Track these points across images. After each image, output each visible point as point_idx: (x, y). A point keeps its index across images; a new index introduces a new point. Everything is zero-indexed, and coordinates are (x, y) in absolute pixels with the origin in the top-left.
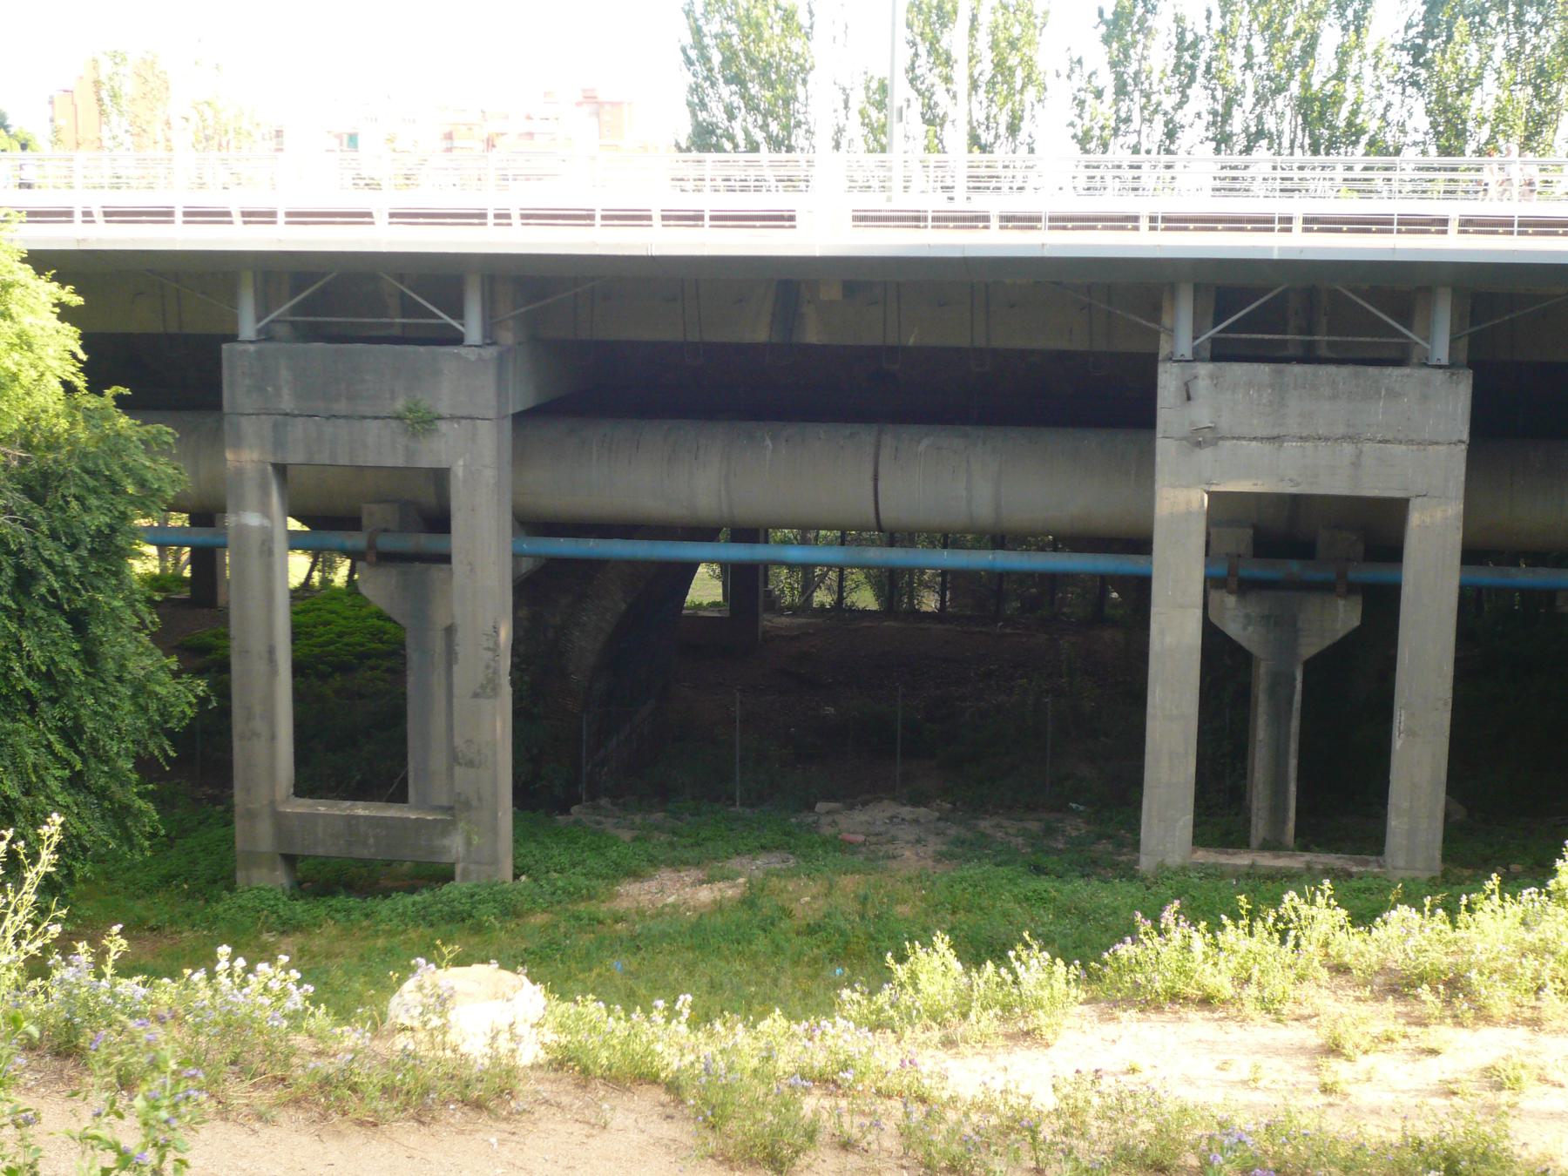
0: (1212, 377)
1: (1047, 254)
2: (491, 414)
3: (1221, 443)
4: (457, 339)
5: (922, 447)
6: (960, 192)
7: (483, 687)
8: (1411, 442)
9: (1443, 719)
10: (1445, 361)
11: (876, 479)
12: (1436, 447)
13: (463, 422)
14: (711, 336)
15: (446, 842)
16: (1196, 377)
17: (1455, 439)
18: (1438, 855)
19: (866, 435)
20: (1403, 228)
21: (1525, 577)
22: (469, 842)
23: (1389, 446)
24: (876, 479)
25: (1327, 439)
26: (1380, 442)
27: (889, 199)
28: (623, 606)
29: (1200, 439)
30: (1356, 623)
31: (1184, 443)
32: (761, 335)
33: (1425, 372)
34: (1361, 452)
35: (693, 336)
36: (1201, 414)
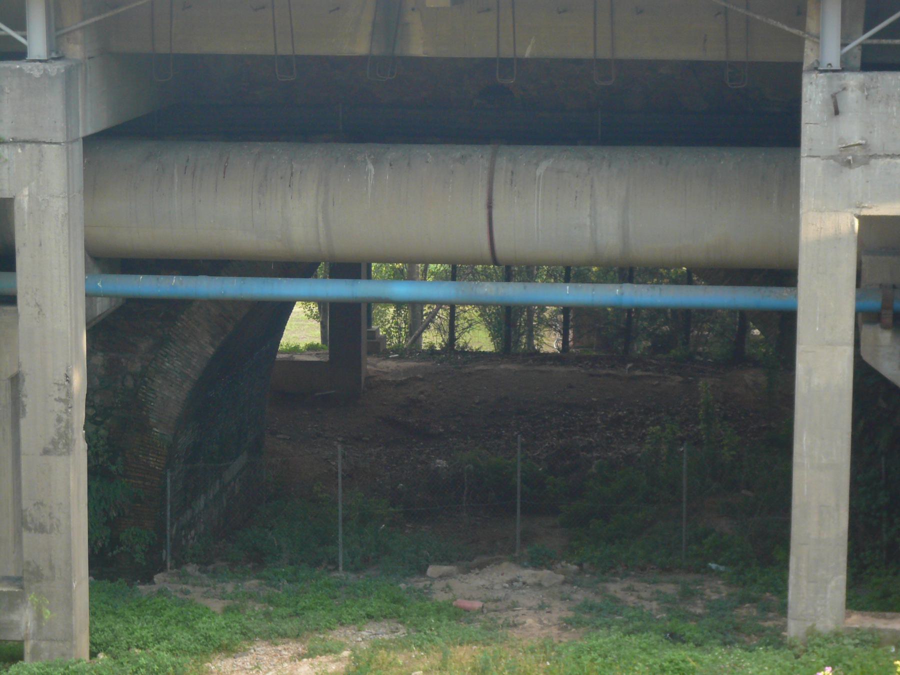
0: (863, 87)
2: (60, 137)
3: (873, 161)
4: (20, 54)
5: (540, 171)
7: (53, 442)
11: (490, 206)
13: (28, 146)
14: (307, 48)
15: (15, 617)
16: (844, 89)
19: (479, 156)
22: (39, 617)
24: (490, 206)
28: (211, 350)
31: (832, 161)
32: (362, 48)
35: (285, 49)
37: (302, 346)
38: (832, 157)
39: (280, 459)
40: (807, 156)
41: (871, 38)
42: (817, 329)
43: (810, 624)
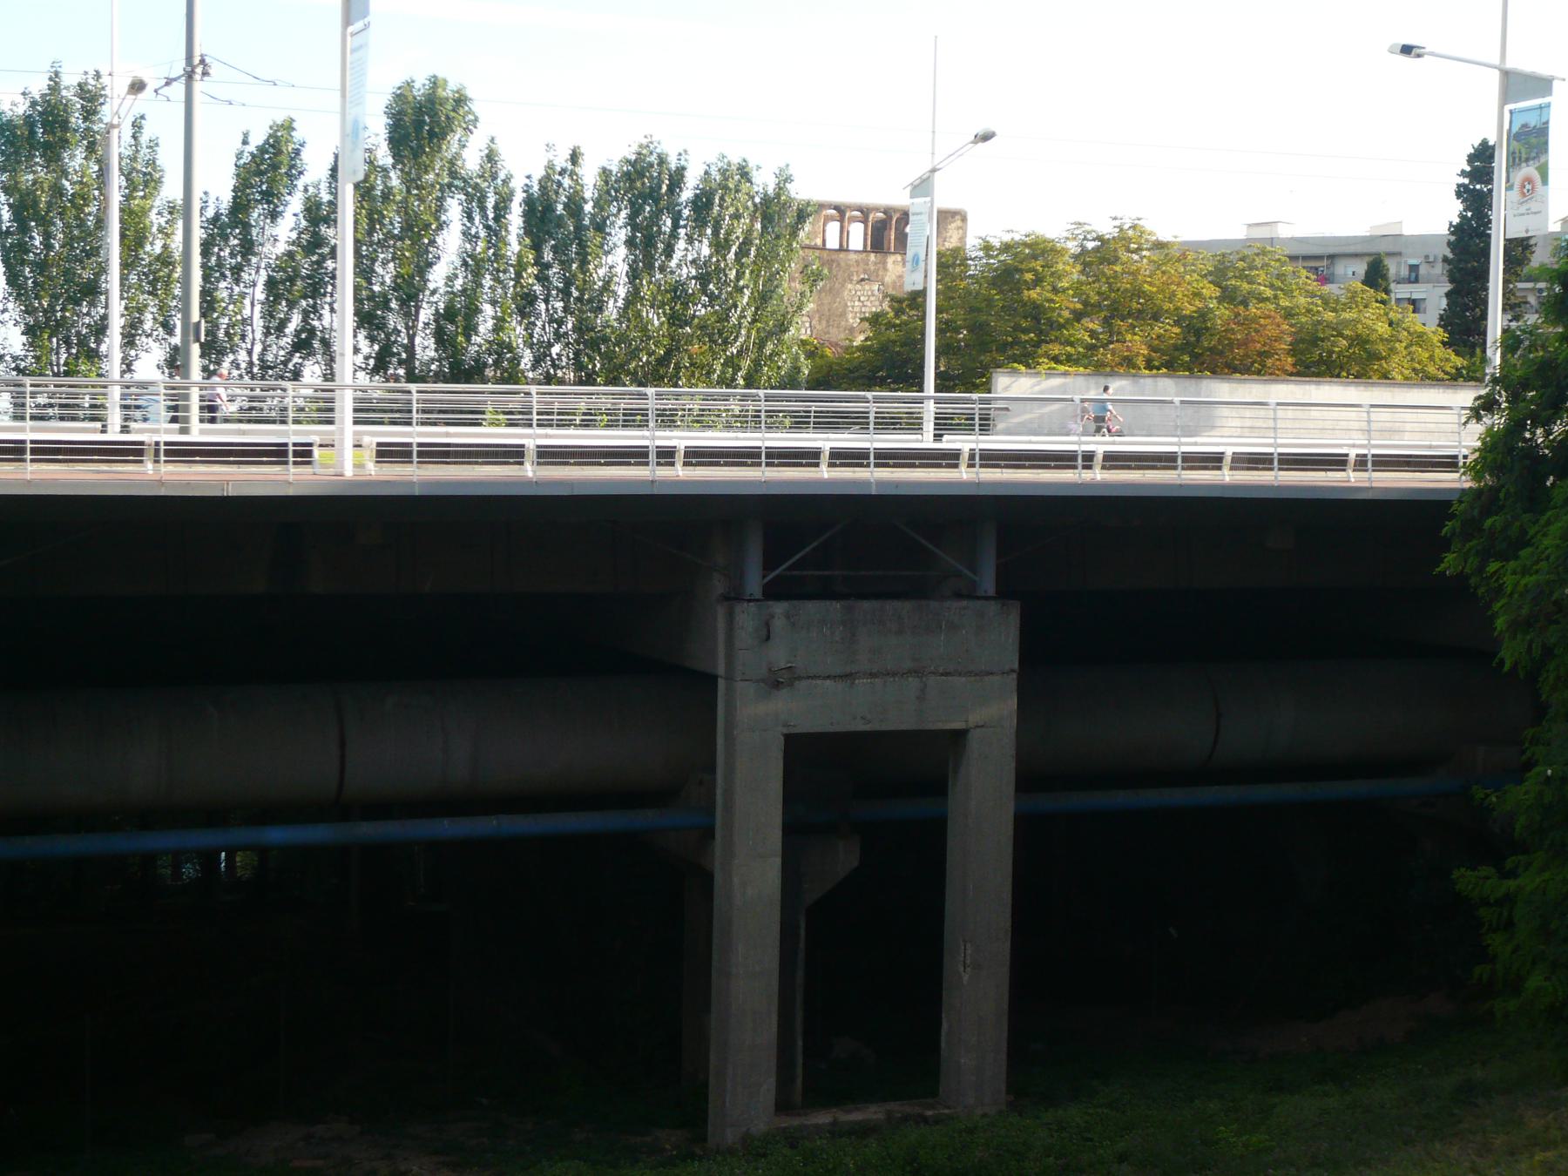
1: (163, 492)
6: (115, 418)
8: (969, 673)
9: (1001, 949)
10: (991, 591)
11: (343, 744)
12: (991, 677)
16: (773, 617)
17: (1007, 668)
18: (1003, 1087)
20: (662, 461)
21: (367, 831)
23: (950, 678)
24: (343, 744)
25: (894, 674)
26: (942, 675)
27: (184, 431)
29: (775, 682)
30: (856, 863)
31: (762, 685)
33: (979, 604)
34: (926, 685)
36: (779, 655)
37: (908, 229)
38: (763, 680)
39: (658, 276)
40: (742, 680)
41: (789, 569)
42: (1172, 931)
43: (744, 1129)
